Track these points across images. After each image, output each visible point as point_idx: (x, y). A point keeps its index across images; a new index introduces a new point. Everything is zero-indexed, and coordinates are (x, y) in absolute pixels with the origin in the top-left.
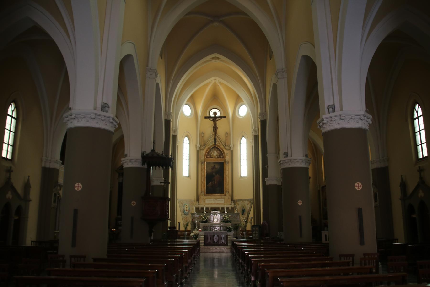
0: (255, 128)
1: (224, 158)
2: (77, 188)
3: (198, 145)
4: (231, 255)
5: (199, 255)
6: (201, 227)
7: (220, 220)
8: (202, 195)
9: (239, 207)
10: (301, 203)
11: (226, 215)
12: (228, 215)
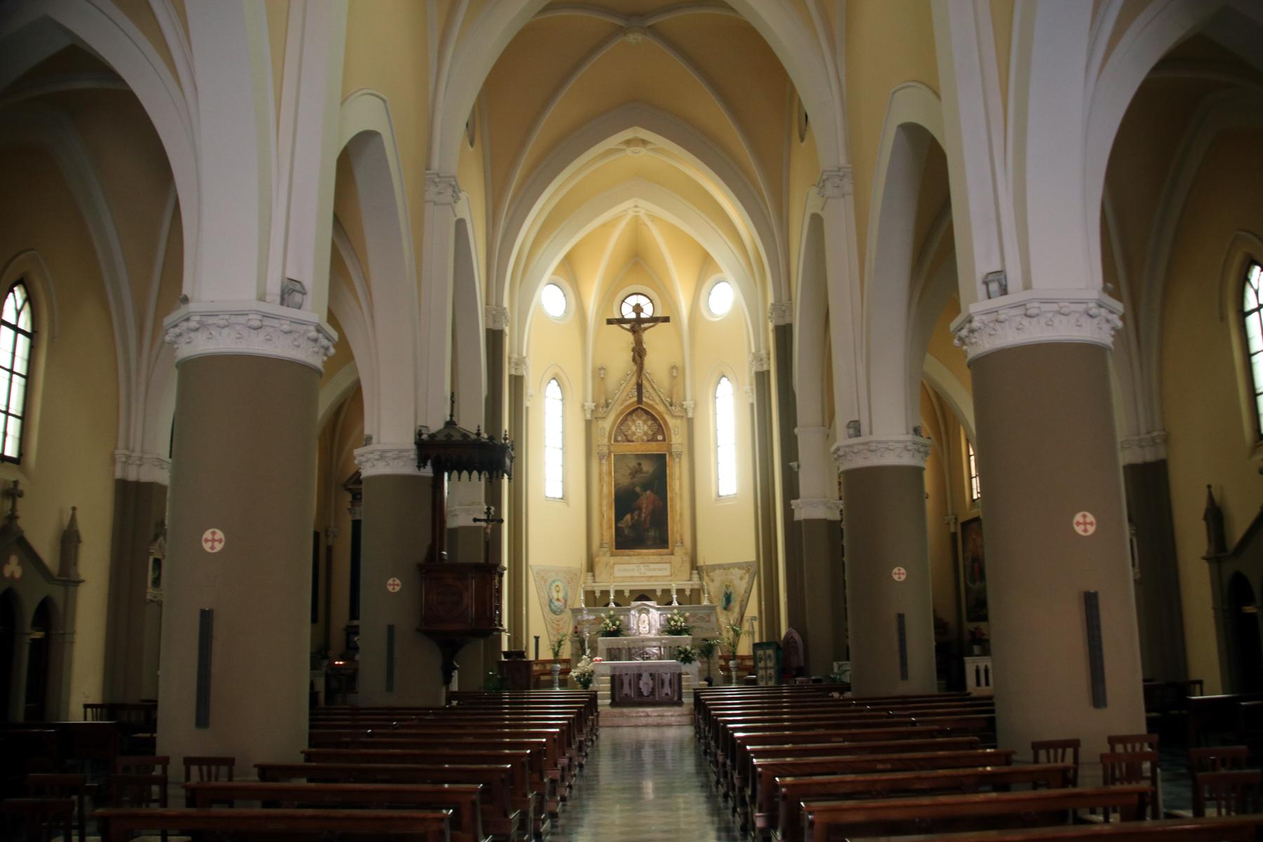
0: (760, 351)
1: (667, 440)
2: (210, 544)
3: (590, 405)
5: (594, 738)
6: (603, 649)
8: (604, 554)
9: (713, 587)
11: (676, 611)
12: (683, 612)
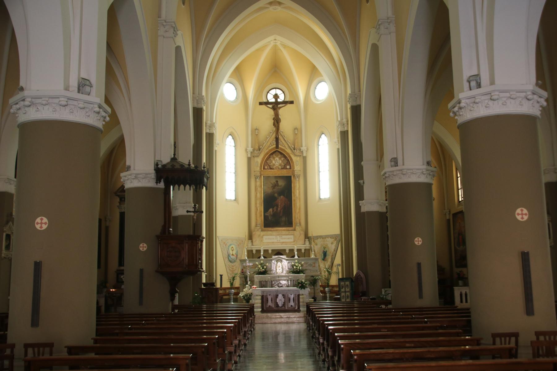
1: (292, 169)
3: (250, 149)
4: (306, 327)
6: (257, 282)
7: (288, 270)
8: (258, 230)
10: (420, 241)
11: (296, 261)
12: (300, 261)
